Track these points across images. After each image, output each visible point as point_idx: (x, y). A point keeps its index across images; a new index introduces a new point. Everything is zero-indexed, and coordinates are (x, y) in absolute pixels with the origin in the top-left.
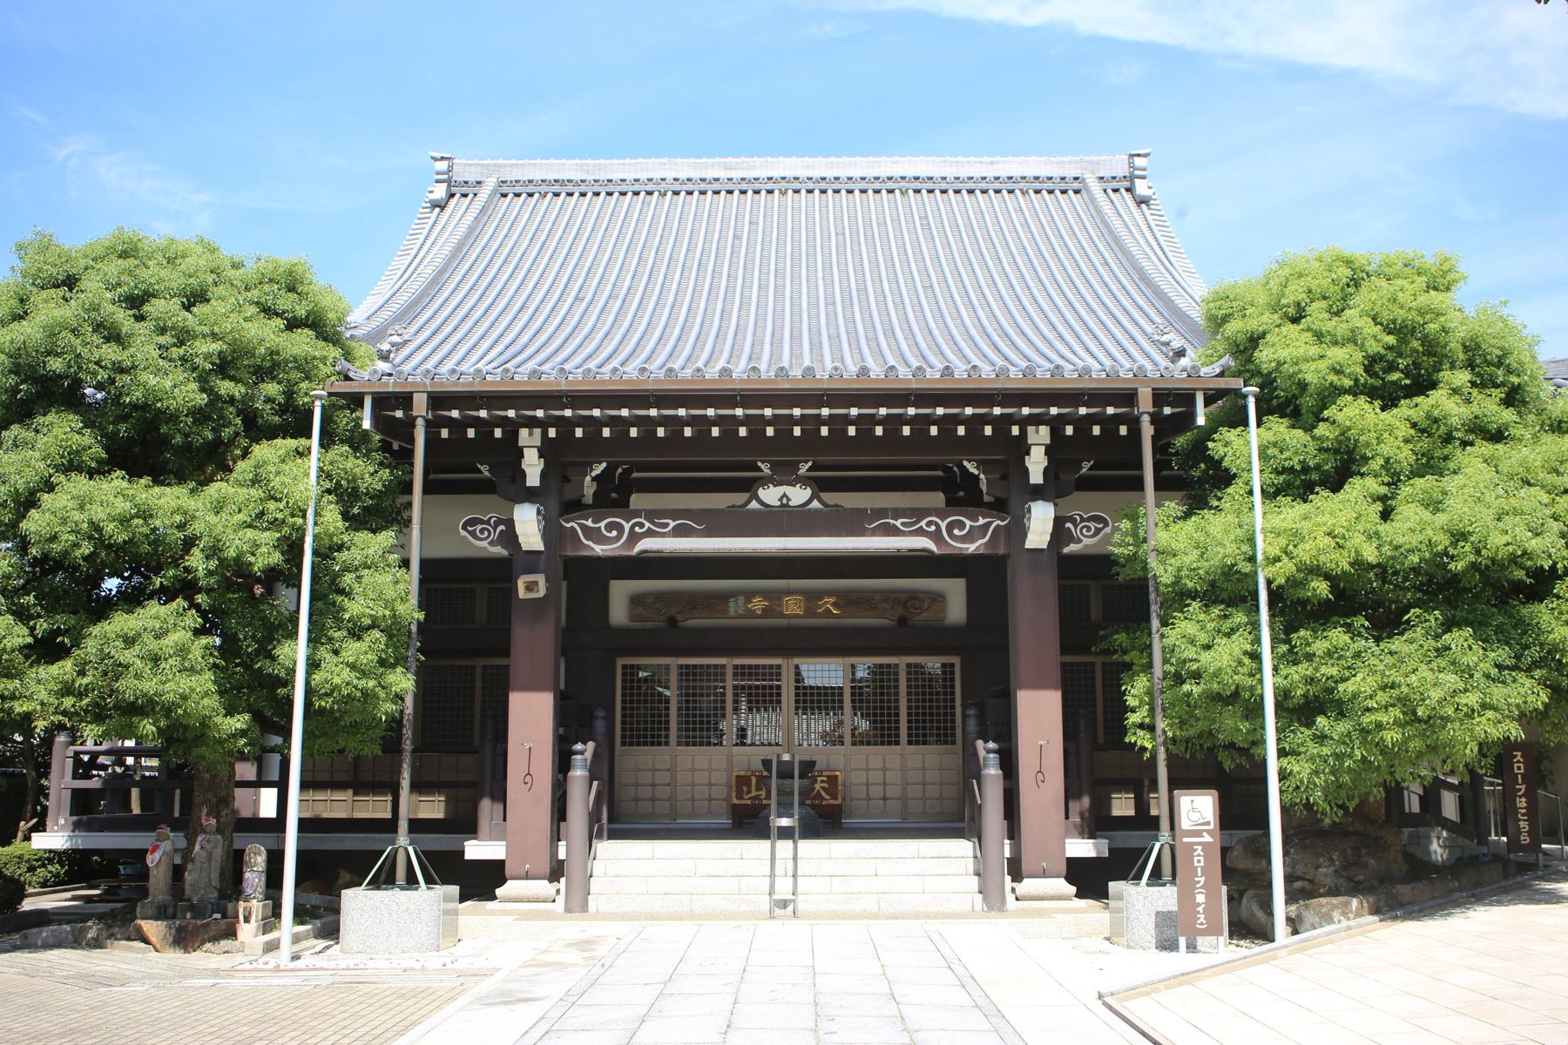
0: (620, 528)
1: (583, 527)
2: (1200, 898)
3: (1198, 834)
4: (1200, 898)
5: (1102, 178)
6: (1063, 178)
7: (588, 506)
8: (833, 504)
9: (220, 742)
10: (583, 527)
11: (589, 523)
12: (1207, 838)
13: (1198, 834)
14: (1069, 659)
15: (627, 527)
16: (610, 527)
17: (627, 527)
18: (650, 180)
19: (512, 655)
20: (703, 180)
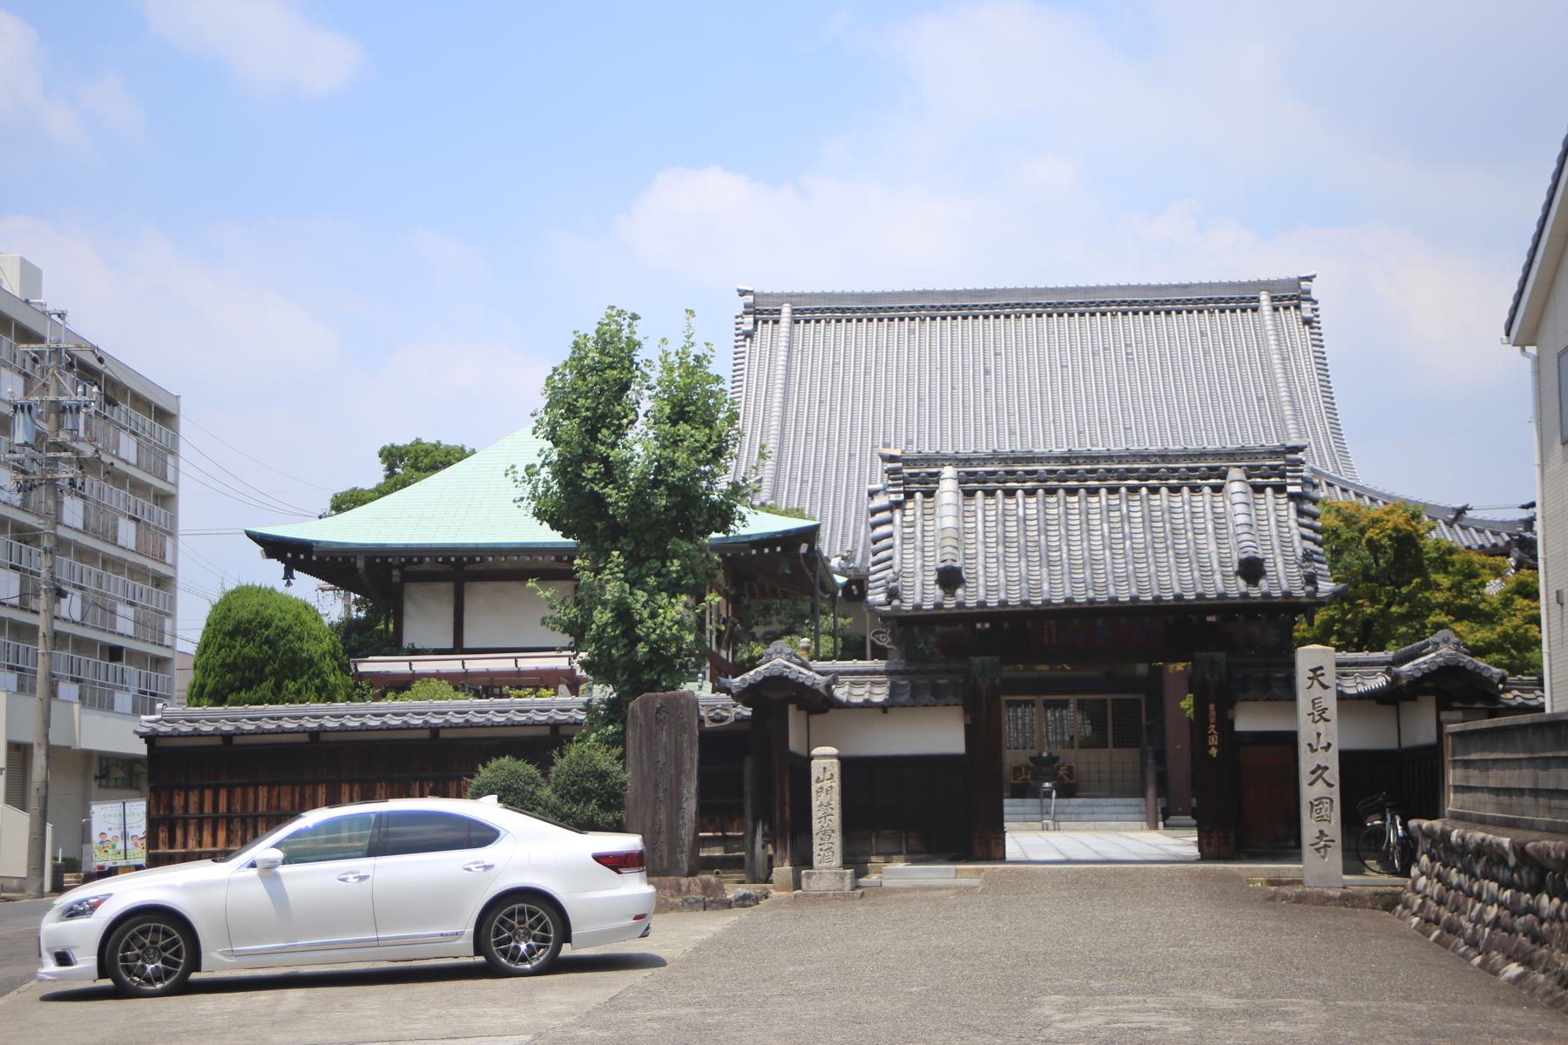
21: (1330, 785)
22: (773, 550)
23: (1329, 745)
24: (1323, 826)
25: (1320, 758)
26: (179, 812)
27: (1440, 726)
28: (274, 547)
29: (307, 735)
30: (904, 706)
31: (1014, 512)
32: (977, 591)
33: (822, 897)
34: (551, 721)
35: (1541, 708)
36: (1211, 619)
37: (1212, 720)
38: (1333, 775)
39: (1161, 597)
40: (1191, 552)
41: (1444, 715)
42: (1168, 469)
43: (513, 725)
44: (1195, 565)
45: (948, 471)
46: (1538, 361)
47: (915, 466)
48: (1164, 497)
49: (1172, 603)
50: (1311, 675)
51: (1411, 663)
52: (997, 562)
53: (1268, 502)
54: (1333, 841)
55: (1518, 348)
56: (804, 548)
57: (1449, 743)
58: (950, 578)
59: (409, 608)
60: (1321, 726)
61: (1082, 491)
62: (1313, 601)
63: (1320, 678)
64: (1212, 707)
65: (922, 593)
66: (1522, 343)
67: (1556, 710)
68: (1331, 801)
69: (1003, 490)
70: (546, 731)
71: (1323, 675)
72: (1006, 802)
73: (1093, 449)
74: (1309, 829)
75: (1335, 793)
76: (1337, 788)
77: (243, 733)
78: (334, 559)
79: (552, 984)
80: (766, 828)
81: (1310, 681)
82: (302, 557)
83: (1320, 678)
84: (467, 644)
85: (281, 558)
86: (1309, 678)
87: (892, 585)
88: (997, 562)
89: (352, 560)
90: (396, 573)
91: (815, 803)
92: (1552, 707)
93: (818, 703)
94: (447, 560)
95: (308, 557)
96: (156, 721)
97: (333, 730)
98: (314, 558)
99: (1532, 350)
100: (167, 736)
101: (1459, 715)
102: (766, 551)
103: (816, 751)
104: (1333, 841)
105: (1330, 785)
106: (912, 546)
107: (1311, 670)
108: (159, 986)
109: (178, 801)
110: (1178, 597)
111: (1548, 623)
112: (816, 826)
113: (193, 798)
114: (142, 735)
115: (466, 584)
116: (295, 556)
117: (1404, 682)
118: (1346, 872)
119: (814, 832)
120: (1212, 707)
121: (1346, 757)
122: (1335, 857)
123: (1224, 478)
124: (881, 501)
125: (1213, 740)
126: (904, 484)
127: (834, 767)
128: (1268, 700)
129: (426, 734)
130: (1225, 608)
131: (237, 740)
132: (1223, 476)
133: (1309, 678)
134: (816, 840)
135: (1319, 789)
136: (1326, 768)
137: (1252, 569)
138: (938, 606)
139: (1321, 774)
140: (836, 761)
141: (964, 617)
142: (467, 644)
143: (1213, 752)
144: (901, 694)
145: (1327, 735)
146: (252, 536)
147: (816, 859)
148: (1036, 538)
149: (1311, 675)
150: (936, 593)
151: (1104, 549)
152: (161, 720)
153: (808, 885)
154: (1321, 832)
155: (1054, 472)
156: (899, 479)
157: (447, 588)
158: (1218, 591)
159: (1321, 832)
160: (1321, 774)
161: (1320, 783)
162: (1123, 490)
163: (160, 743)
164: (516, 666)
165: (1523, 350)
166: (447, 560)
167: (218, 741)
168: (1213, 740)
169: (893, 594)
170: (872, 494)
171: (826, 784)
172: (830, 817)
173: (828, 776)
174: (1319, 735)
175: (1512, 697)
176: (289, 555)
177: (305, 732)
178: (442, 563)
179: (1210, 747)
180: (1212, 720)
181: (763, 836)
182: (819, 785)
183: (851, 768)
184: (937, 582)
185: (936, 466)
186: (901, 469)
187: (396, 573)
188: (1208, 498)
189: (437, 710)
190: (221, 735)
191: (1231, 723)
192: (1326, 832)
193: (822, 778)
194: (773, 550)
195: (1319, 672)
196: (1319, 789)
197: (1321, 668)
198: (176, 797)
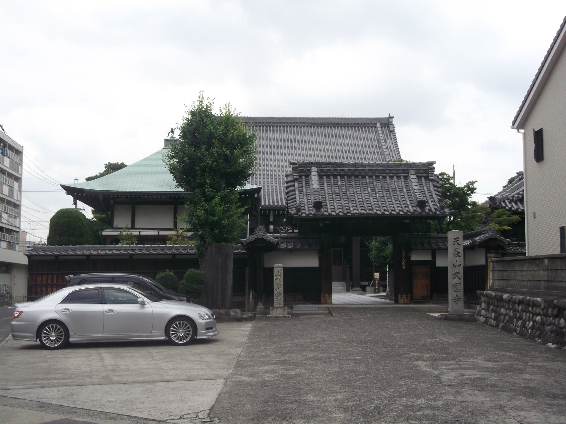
0: (286, 228)
1: (279, 228)
2: (377, 287)
3: (377, 278)
4: (377, 287)
5: (381, 123)
6: (371, 123)
7: (546, 258)
8: (96, 386)
9: (437, 176)
10: (279, 228)
11: (280, 227)
12: (378, 279)
13: (377, 278)
14: (251, 183)
15: (287, 228)
16: (284, 228)
17: (287, 228)
18: (267, 123)
19: (187, 303)
20: (280, 123)
21: (460, 279)
22: (245, 195)
23: (460, 265)
24: (458, 293)
25: (457, 270)
26: (39, 283)
27: (487, 258)
28: (69, 190)
29: (171, 256)
30: (307, 250)
31: (337, 183)
32: (327, 210)
33: (277, 318)
34: (173, 254)
35: (525, 254)
36: (327, 222)
37: (404, 256)
38: (461, 275)
39: (384, 213)
40: (399, 198)
41: (489, 255)
42: (340, 169)
43: (47, 256)
44: (401, 203)
45: (314, 169)
46: (525, 134)
47: (302, 167)
48: (339, 180)
49: (396, 215)
50: (454, 240)
51: (479, 237)
52: (333, 200)
53: (423, 182)
54: (461, 298)
55: (517, 130)
56: (256, 195)
57: (491, 265)
58: (318, 205)
59: (116, 213)
60: (458, 258)
61: (360, 177)
62: (443, 215)
63: (458, 242)
64: (404, 251)
65: (308, 211)
66: (518, 128)
67: (530, 255)
68: (460, 284)
69: (347, 176)
70: (171, 257)
71: (458, 240)
72: (333, 283)
73: (376, 162)
74: (451, 294)
75: (462, 282)
76: (462, 280)
77: (63, 256)
78: (131, 196)
79: (71, 352)
80: (253, 292)
81: (454, 243)
82: (80, 194)
83: (458, 242)
84: (136, 226)
85: (72, 195)
86: (454, 241)
87: (298, 207)
88: (333, 200)
89: (98, 196)
90: (112, 201)
91: (275, 284)
92: (528, 254)
93: (270, 247)
94: (175, 197)
95: (82, 195)
96: (32, 250)
97: (95, 255)
98: (84, 195)
99: (522, 131)
100: (35, 256)
101: (493, 255)
102: (243, 196)
103: (275, 266)
104: (461, 298)
105: (460, 279)
106: (303, 194)
107: (454, 239)
108: (185, 341)
109: (39, 279)
110: (398, 213)
111: (528, 224)
112: (275, 292)
113: (45, 278)
114: (26, 255)
115: (178, 206)
116: (78, 194)
117: (477, 243)
118: (464, 308)
119: (274, 294)
120: (404, 251)
121: (466, 269)
122: (461, 304)
123: (408, 174)
124: (290, 179)
125: (404, 263)
126: (299, 173)
127: (282, 272)
128: (424, 249)
129: (128, 257)
130: (413, 218)
131: (60, 258)
132: (408, 173)
133: (454, 241)
134: (275, 297)
135: (456, 280)
136: (459, 273)
137: (422, 204)
138: (315, 215)
139: (457, 275)
140: (282, 269)
141: (324, 219)
142: (136, 226)
143: (404, 267)
144: (297, 246)
145: (459, 262)
146: (63, 186)
147: (275, 303)
148: (346, 192)
149: (454, 240)
150: (314, 211)
151: (369, 197)
152: (33, 250)
153: (272, 313)
154: (457, 295)
155: (351, 170)
156: (297, 171)
157: (172, 206)
158: (329, 213)
159: (457, 295)
160: (457, 275)
161: (457, 278)
162: (374, 177)
163: (32, 258)
164: (158, 233)
165: (518, 131)
166: (126, 197)
167: (53, 258)
168: (404, 263)
169: (299, 210)
170: (287, 176)
171: (279, 277)
172: (280, 289)
173: (280, 274)
174: (457, 261)
175: (511, 249)
176: (75, 194)
177: (85, 255)
178: (168, 198)
179: (403, 265)
180: (404, 256)
181: (253, 295)
182: (277, 277)
183: (287, 271)
184: (313, 207)
185: (309, 167)
186: (297, 167)
187: (112, 201)
188: (403, 180)
189: (102, 249)
190: (130, 255)
191: (410, 257)
192: (458, 295)
193: (277, 275)
194: (245, 195)
195: (457, 240)
196: (456, 280)
197: (458, 238)
198: (38, 277)
